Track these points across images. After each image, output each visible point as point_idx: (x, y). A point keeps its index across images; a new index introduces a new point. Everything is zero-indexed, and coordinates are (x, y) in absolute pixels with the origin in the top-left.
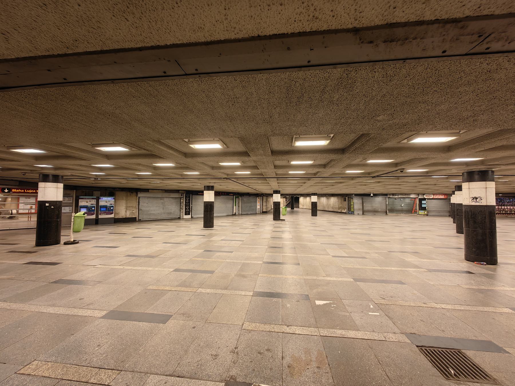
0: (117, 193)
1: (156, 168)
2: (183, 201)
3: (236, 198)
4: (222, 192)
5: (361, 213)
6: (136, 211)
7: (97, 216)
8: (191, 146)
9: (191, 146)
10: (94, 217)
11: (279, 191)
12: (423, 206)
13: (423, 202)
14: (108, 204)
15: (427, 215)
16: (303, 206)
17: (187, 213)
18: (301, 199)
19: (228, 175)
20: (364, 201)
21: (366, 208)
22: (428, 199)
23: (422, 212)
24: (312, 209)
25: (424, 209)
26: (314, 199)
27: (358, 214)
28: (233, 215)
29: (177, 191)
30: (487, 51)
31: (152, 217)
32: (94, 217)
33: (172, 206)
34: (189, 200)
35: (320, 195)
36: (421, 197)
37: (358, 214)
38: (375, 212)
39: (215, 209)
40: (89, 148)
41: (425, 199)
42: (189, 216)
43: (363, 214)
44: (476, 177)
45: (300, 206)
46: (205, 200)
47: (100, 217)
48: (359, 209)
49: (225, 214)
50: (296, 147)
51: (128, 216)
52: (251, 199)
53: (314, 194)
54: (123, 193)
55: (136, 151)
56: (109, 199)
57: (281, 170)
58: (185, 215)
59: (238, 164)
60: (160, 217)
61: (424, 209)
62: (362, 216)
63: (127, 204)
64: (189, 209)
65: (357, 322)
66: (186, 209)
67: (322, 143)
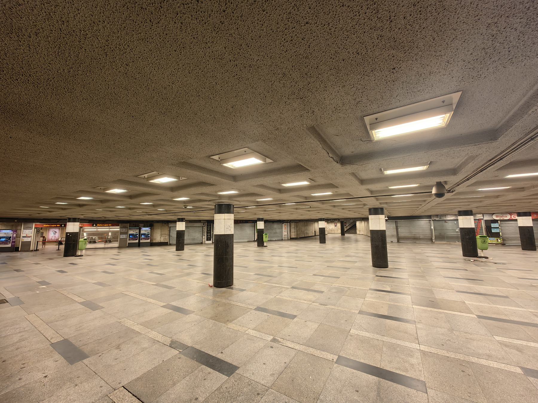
0: (156, 225)
4: (241, 220)
5: (395, 240)
6: (167, 237)
7: (139, 241)
8: (225, 165)
9: (225, 165)
10: (149, 241)
11: (471, 211)
12: (493, 231)
13: (493, 225)
14: (146, 233)
15: (503, 245)
16: (360, 231)
18: (358, 223)
19: (306, 198)
21: (401, 235)
22: (501, 221)
23: (490, 240)
24: (325, 235)
25: (497, 235)
26: (322, 224)
29: (199, 221)
32: (137, 241)
34: (210, 228)
35: (328, 220)
36: (487, 218)
37: (392, 242)
38: (415, 239)
39: (186, 237)
40: (102, 191)
41: (495, 221)
43: (398, 242)
44: (72, 220)
45: (358, 232)
47: (141, 241)
48: (393, 236)
49: (247, 241)
50: (379, 142)
51: (162, 241)
52: (276, 226)
53: (321, 220)
54: (159, 224)
56: (147, 229)
58: (207, 240)
61: (497, 235)
62: (396, 244)
63: (161, 232)
64: (210, 235)
66: (207, 236)
67: (434, 122)
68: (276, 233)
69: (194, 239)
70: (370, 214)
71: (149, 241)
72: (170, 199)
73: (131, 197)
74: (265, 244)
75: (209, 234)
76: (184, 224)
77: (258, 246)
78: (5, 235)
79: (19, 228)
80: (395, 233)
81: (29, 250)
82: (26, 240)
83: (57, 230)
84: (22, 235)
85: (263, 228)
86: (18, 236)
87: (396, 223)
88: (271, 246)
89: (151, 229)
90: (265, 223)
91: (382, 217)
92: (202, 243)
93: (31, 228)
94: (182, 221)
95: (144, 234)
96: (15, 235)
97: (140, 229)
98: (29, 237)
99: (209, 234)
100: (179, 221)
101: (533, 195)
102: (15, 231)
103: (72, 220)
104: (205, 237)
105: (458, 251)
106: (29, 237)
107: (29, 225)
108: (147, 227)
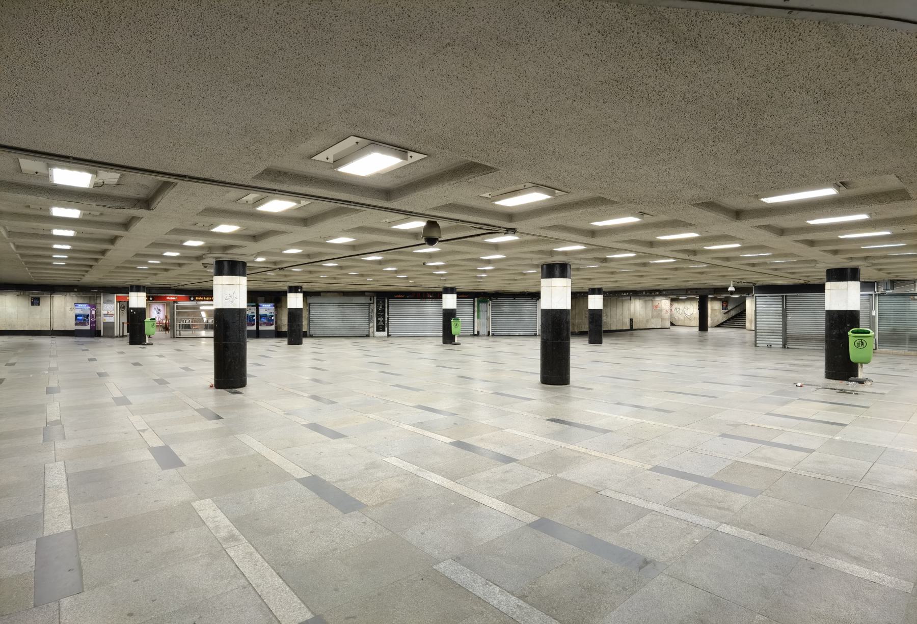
1: (593, 233)
2: (374, 307)
3: (479, 302)
7: (257, 327)
14: (268, 313)
17: (380, 328)
20: (789, 306)
27: (769, 346)
28: (474, 335)
29: (361, 294)
30: (193, 228)
31: (328, 333)
33: (358, 317)
34: (384, 307)
37: (769, 346)
42: (385, 334)
43: (784, 346)
44: (557, 272)
46: (827, 308)
48: (772, 332)
55: (563, 198)
57: (792, 216)
58: (378, 330)
59: (829, 192)
60: (338, 333)
64: (384, 321)
65: (504, 609)
66: (378, 321)
68: (520, 320)
69: (353, 328)
70: (829, 280)
71: (273, 328)
72: (321, 240)
73: (306, 221)
74: (457, 340)
75: (381, 319)
76: (143, 295)
77: (445, 342)
78: (81, 312)
79: (98, 301)
80: (780, 326)
81: (112, 336)
82: (109, 319)
83: (161, 307)
84: (103, 312)
85: (454, 307)
86: (98, 314)
87: (785, 301)
88: (468, 346)
89: (276, 307)
90: (304, 296)
91: (854, 286)
92: (368, 336)
93: (111, 302)
94: (296, 292)
95: (265, 316)
96: (93, 312)
97: (257, 307)
98: (112, 315)
99: (381, 319)
100: (291, 292)
101: (413, 266)
102: (93, 306)
103: (557, 272)
104: (374, 324)
105: (815, 364)
106: (112, 315)
107: (110, 297)
108: (271, 302)
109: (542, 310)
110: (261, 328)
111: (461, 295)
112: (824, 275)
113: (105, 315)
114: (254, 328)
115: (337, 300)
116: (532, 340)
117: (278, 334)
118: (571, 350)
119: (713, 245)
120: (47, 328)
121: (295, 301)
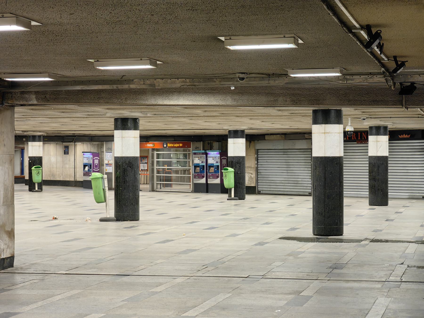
31: (273, 189)
46: (370, 154)
60: (282, 189)
76: (242, 141)
85: (341, 154)
95: (212, 166)
96: (96, 162)
109: (29, 157)
110: (210, 181)
111: (395, 135)
112: (111, 124)
113: (248, 167)
114: (203, 181)
115: (280, 145)
116: (363, 200)
117: (224, 190)
118: (346, 211)
119: (327, 79)
120: (72, 179)
121: (237, 147)
